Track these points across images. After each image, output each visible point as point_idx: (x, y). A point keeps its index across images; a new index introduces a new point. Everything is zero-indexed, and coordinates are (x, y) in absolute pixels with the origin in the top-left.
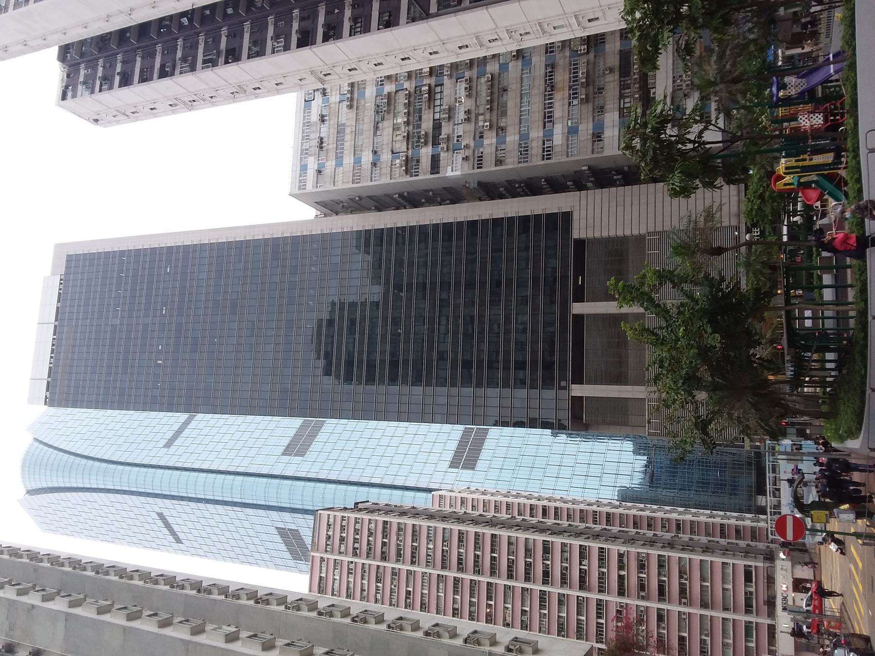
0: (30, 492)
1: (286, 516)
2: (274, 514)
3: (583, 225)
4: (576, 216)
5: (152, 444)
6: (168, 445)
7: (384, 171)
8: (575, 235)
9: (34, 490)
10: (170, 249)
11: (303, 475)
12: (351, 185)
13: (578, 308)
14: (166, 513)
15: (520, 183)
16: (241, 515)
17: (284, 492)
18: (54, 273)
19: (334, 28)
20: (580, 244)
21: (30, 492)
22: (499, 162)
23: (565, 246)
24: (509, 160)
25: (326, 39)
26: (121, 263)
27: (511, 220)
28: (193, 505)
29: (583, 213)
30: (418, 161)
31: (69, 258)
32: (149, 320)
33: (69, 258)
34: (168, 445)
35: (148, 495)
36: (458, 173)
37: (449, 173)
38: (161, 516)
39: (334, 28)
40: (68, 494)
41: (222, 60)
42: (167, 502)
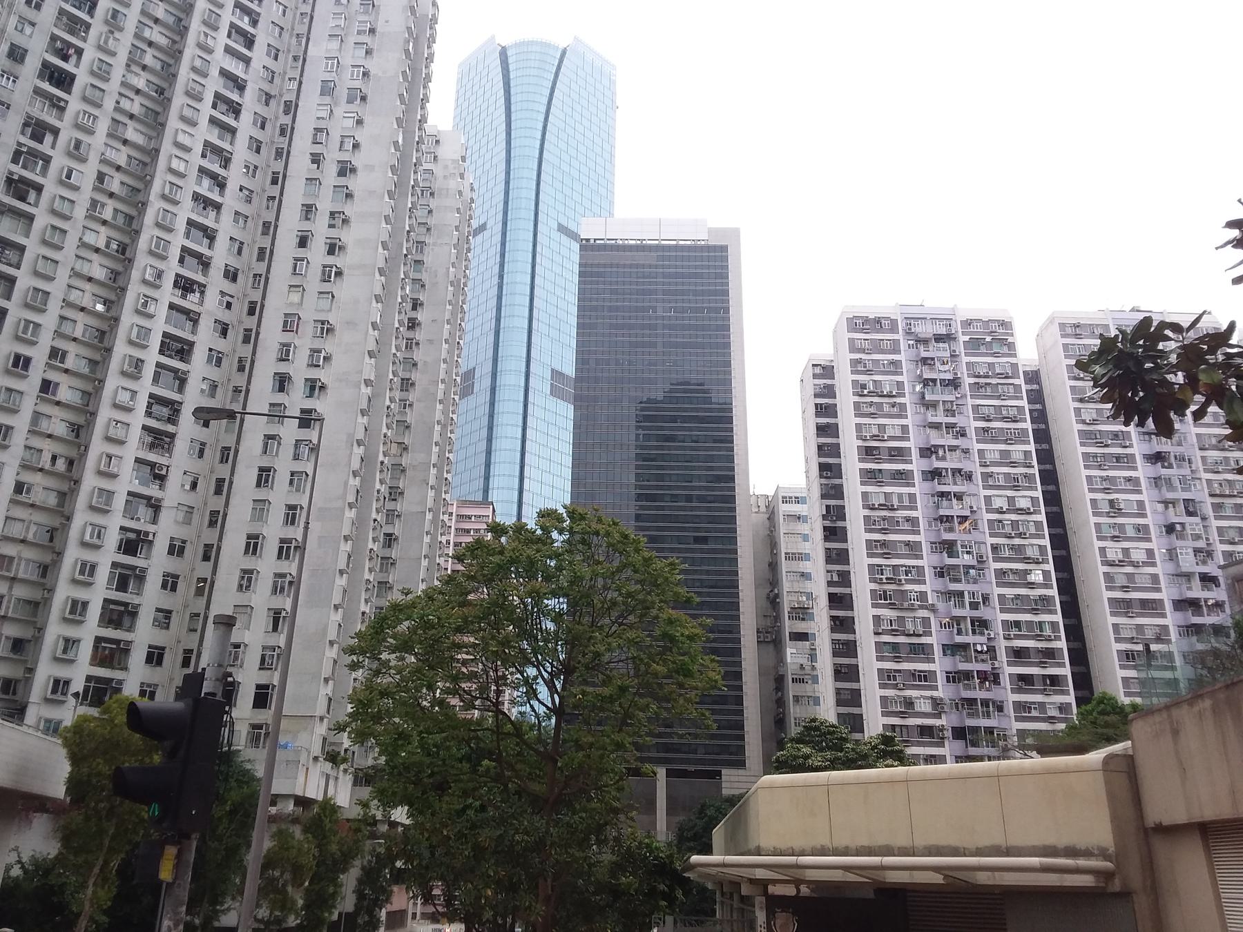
0: (503, 53)
1: (487, 382)
2: (488, 367)
3: (733, 779)
4: (741, 772)
5: (561, 208)
6: (562, 229)
7: (796, 584)
8: (724, 772)
9: (507, 58)
10: (728, 364)
11: (531, 399)
12: (783, 551)
13: (661, 772)
14: (487, 233)
15: (784, 713)
16: (491, 262)
17: (511, 380)
18: (710, 231)
19: (842, 624)
20: (719, 774)
21: (503, 53)
22: (797, 699)
23: (715, 762)
24: (798, 709)
25: (833, 618)
26: (717, 310)
27: (741, 713)
28: (496, 269)
29: (744, 779)
30: (803, 619)
31: (724, 249)
32: (660, 349)
33: (724, 249)
34: (562, 229)
35: (505, 213)
36: (789, 660)
37: (789, 651)
38: (482, 228)
39: (842, 624)
40: (502, 100)
41: (828, 523)
42: (498, 238)
